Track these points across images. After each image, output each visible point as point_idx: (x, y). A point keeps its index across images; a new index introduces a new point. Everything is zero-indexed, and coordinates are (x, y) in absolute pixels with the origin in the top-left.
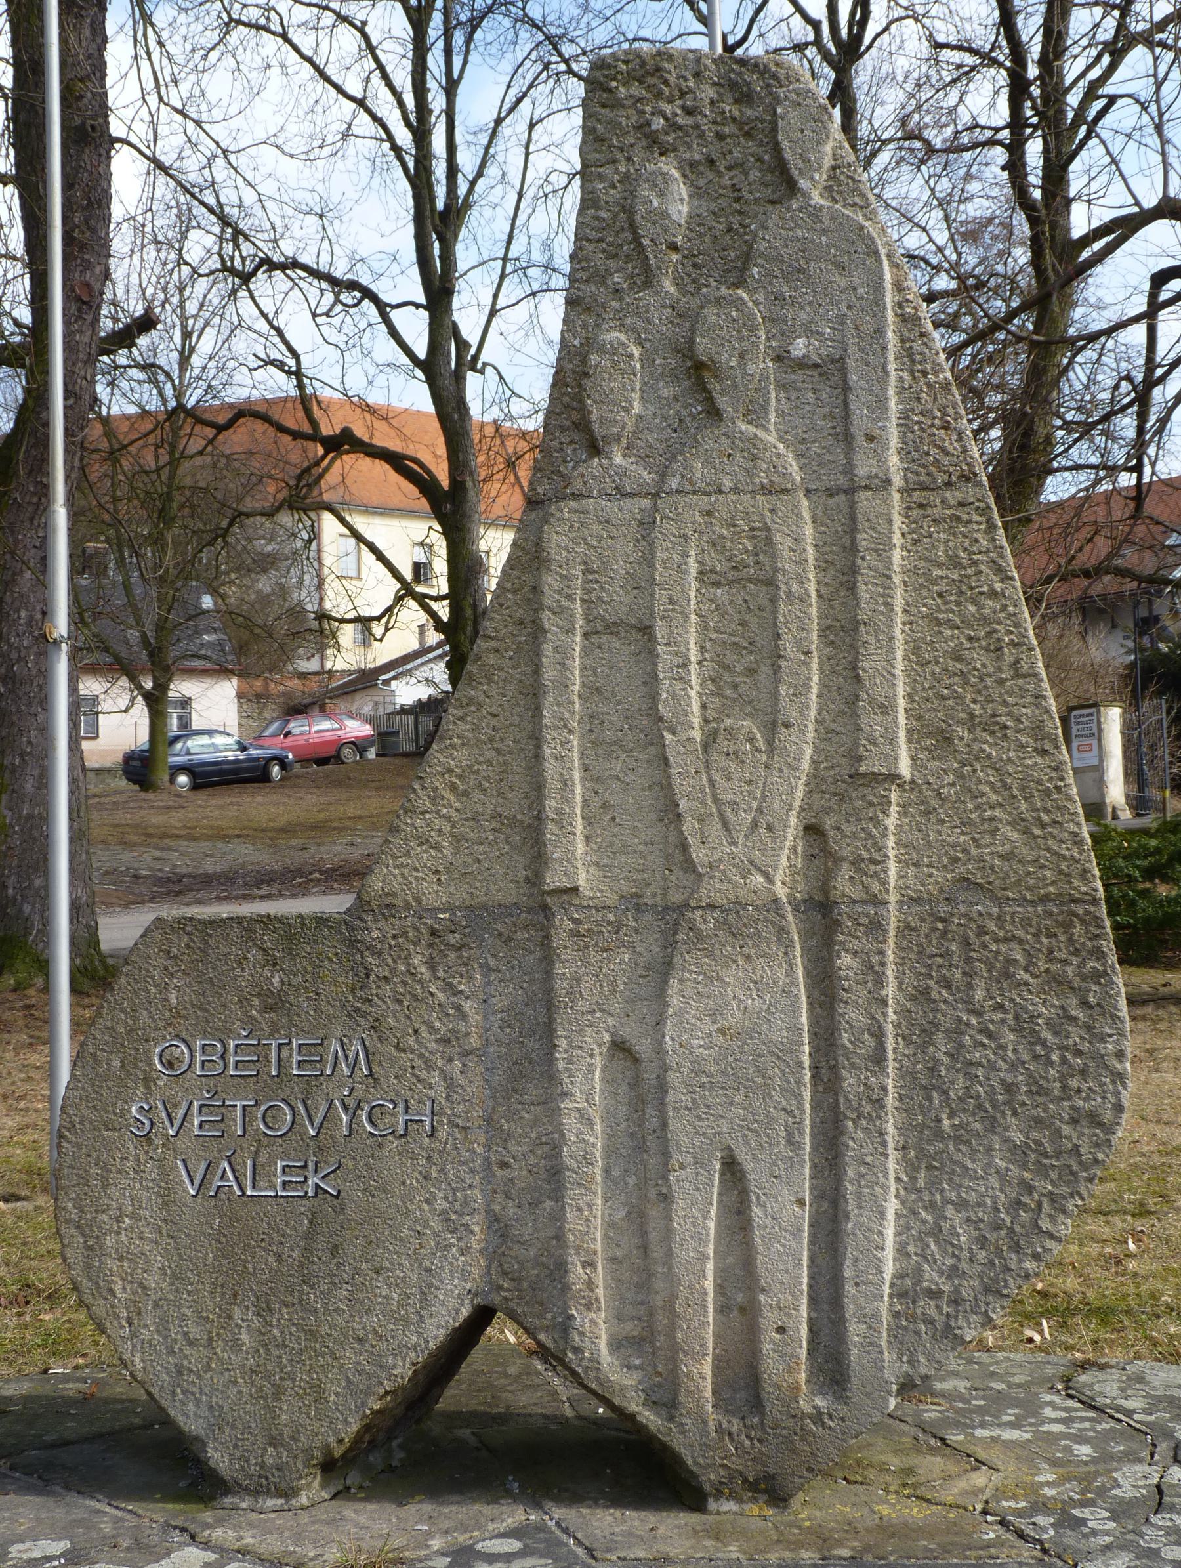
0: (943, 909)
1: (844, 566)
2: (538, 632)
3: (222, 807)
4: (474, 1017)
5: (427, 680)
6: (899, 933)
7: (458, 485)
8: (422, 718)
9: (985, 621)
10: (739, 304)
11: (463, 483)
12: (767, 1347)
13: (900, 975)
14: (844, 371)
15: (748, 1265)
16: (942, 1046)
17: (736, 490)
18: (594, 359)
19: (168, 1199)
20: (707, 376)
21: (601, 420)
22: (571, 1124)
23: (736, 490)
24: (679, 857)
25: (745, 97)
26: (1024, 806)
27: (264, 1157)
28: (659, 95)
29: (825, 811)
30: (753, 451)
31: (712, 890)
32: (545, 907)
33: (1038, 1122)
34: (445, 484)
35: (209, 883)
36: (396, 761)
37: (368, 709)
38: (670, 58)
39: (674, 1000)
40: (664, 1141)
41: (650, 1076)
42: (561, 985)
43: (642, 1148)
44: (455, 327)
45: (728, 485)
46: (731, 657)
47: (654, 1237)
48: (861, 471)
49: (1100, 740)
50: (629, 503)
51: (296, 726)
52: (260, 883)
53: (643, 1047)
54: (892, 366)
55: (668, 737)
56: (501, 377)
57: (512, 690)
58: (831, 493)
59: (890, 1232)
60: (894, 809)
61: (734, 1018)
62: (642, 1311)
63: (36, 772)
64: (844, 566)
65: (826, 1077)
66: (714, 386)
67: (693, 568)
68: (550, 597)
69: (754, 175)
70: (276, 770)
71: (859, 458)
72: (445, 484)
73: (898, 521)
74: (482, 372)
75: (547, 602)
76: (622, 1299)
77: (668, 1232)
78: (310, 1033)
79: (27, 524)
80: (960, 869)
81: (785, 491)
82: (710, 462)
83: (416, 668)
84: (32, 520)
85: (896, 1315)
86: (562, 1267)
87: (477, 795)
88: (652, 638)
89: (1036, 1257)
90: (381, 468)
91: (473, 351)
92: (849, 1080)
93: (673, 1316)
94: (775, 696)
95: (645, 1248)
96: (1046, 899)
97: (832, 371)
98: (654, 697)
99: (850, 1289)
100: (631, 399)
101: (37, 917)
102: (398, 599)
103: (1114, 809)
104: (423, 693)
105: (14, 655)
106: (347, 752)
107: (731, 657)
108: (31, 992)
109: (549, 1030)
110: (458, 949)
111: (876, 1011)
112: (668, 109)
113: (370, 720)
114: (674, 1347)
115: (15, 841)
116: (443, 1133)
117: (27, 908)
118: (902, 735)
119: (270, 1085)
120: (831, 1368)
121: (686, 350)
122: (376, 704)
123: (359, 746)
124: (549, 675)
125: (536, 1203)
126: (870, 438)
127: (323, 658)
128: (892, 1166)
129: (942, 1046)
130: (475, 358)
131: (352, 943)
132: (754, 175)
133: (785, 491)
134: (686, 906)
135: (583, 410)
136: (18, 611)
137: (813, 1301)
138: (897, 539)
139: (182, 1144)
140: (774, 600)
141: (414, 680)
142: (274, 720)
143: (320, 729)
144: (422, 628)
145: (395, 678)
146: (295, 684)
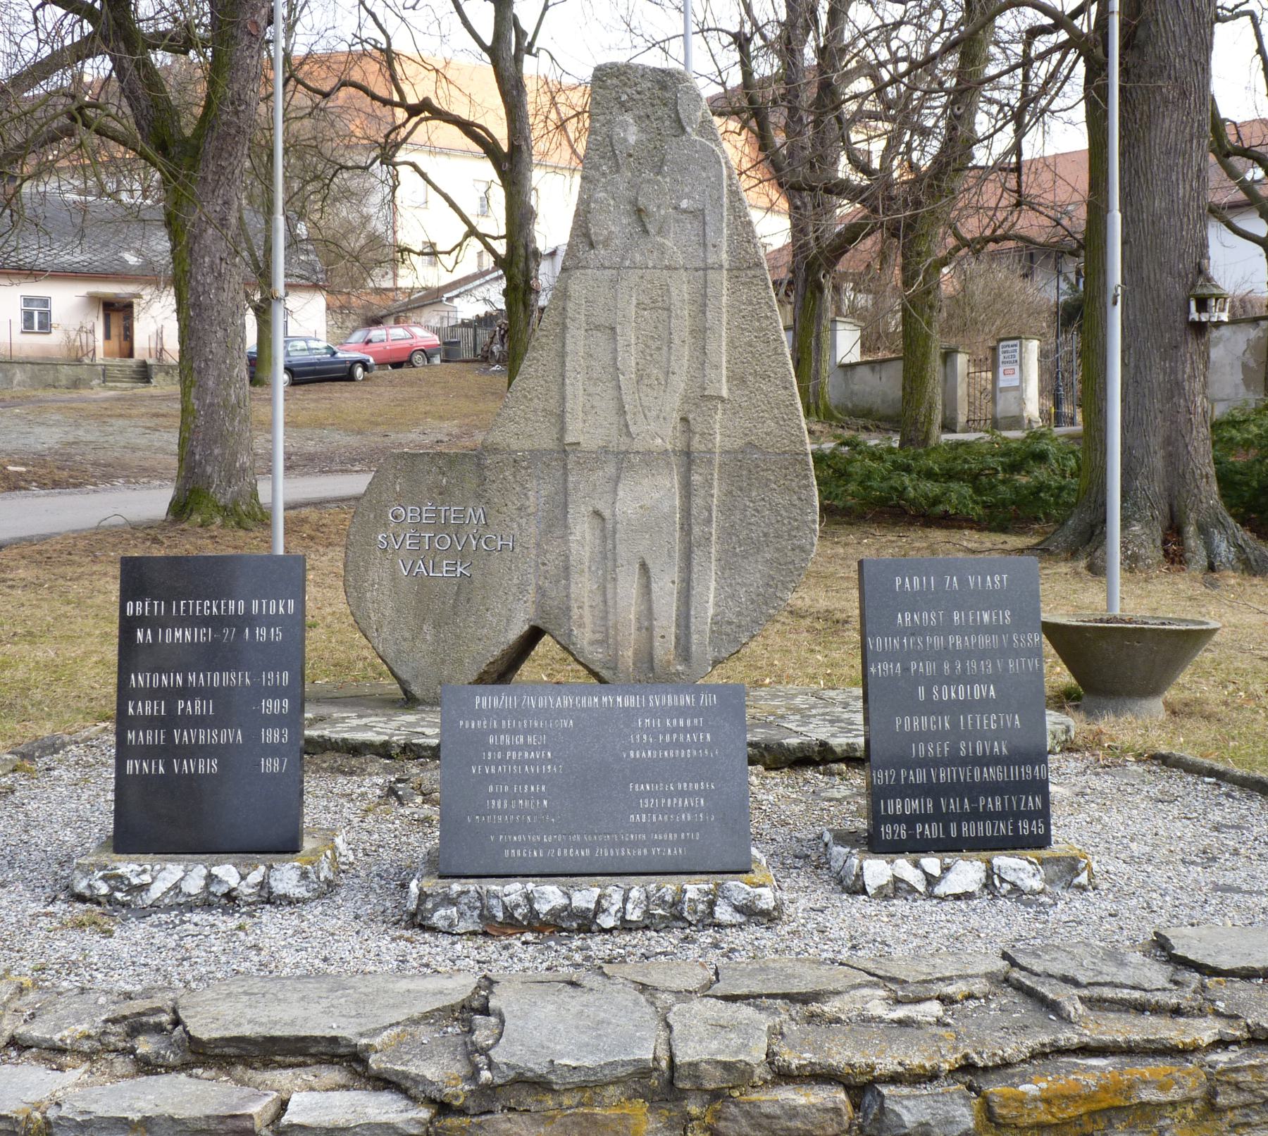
0: (740, 457)
1: (701, 303)
2: (564, 328)
3: (316, 401)
4: (532, 499)
5: (484, 299)
6: (720, 466)
7: (515, 148)
8: (479, 331)
9: (762, 329)
10: (658, 183)
11: (519, 147)
12: (656, 644)
13: (720, 485)
14: (703, 215)
15: (650, 609)
16: (738, 515)
17: (654, 267)
18: (593, 205)
19: (394, 577)
20: (643, 215)
21: (596, 234)
22: (573, 546)
23: (654, 267)
24: (624, 430)
25: (664, 87)
26: (776, 411)
27: (437, 559)
28: (625, 84)
29: (689, 411)
30: (662, 250)
31: (638, 445)
32: (565, 451)
33: (778, 550)
34: (505, 147)
35: (312, 460)
36: (458, 365)
37: (435, 322)
38: (631, 68)
39: (621, 493)
40: (614, 554)
41: (609, 526)
42: (571, 486)
43: (605, 558)
44: (515, 19)
45: (651, 265)
46: (650, 342)
47: (609, 596)
48: (710, 261)
49: (1021, 366)
50: (607, 272)
51: (376, 333)
52: (353, 461)
53: (607, 514)
54: (725, 214)
55: (621, 377)
56: (552, 58)
57: (553, 354)
58: (697, 270)
59: (712, 596)
60: (720, 412)
61: (647, 502)
62: (603, 629)
63: (216, 373)
64: (701, 303)
65: (686, 528)
66: (646, 220)
67: (634, 302)
68: (570, 313)
69: (667, 123)
70: (359, 371)
71: (709, 255)
72: (505, 147)
73: (725, 283)
74: (535, 55)
75: (570, 315)
76: (595, 624)
77: (615, 593)
78: (459, 505)
79: (210, 195)
80: (748, 439)
81: (676, 269)
82: (643, 254)
83: (475, 288)
84: (213, 192)
85: (713, 632)
86: (569, 609)
87: (536, 401)
88: (615, 333)
89: (774, 608)
90: (454, 130)
91: (529, 39)
92: (696, 530)
93: (616, 629)
94: (669, 361)
95: (605, 602)
96: (785, 452)
97: (698, 215)
98: (615, 359)
99: (693, 620)
100: (613, 224)
101: (216, 476)
102: (467, 236)
103: (1030, 421)
104: (481, 310)
105: (200, 289)
106: (418, 358)
107: (650, 342)
108: (213, 527)
109: (566, 505)
110: (526, 469)
111: (709, 499)
112: (629, 91)
113: (437, 331)
114: (616, 643)
115: (201, 421)
116: (517, 550)
117: (209, 469)
118: (724, 379)
119: (441, 527)
120: (684, 652)
121: (634, 202)
122: (442, 318)
123: (427, 353)
124: (569, 348)
125: (558, 581)
126: (714, 246)
127: (395, 276)
128: (713, 568)
129: (738, 515)
130: (531, 44)
131: (479, 465)
132: (667, 123)
133: (676, 269)
134: (627, 452)
135: (587, 228)
136: (203, 257)
137: (678, 626)
138: (725, 292)
139: (402, 552)
140: (669, 317)
141: (473, 299)
142: (354, 330)
143: (392, 336)
144: (480, 254)
145: (457, 296)
146: (375, 299)
